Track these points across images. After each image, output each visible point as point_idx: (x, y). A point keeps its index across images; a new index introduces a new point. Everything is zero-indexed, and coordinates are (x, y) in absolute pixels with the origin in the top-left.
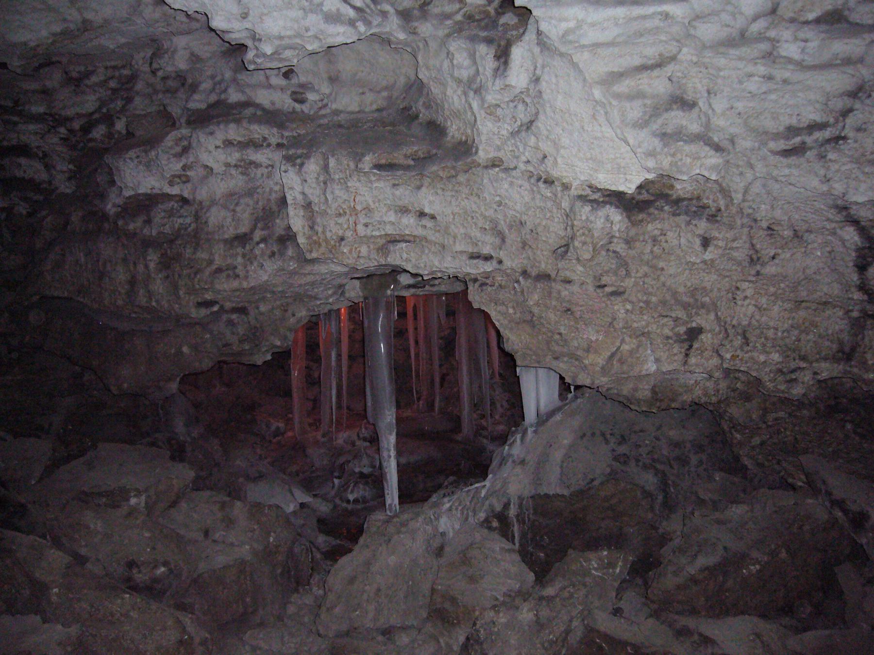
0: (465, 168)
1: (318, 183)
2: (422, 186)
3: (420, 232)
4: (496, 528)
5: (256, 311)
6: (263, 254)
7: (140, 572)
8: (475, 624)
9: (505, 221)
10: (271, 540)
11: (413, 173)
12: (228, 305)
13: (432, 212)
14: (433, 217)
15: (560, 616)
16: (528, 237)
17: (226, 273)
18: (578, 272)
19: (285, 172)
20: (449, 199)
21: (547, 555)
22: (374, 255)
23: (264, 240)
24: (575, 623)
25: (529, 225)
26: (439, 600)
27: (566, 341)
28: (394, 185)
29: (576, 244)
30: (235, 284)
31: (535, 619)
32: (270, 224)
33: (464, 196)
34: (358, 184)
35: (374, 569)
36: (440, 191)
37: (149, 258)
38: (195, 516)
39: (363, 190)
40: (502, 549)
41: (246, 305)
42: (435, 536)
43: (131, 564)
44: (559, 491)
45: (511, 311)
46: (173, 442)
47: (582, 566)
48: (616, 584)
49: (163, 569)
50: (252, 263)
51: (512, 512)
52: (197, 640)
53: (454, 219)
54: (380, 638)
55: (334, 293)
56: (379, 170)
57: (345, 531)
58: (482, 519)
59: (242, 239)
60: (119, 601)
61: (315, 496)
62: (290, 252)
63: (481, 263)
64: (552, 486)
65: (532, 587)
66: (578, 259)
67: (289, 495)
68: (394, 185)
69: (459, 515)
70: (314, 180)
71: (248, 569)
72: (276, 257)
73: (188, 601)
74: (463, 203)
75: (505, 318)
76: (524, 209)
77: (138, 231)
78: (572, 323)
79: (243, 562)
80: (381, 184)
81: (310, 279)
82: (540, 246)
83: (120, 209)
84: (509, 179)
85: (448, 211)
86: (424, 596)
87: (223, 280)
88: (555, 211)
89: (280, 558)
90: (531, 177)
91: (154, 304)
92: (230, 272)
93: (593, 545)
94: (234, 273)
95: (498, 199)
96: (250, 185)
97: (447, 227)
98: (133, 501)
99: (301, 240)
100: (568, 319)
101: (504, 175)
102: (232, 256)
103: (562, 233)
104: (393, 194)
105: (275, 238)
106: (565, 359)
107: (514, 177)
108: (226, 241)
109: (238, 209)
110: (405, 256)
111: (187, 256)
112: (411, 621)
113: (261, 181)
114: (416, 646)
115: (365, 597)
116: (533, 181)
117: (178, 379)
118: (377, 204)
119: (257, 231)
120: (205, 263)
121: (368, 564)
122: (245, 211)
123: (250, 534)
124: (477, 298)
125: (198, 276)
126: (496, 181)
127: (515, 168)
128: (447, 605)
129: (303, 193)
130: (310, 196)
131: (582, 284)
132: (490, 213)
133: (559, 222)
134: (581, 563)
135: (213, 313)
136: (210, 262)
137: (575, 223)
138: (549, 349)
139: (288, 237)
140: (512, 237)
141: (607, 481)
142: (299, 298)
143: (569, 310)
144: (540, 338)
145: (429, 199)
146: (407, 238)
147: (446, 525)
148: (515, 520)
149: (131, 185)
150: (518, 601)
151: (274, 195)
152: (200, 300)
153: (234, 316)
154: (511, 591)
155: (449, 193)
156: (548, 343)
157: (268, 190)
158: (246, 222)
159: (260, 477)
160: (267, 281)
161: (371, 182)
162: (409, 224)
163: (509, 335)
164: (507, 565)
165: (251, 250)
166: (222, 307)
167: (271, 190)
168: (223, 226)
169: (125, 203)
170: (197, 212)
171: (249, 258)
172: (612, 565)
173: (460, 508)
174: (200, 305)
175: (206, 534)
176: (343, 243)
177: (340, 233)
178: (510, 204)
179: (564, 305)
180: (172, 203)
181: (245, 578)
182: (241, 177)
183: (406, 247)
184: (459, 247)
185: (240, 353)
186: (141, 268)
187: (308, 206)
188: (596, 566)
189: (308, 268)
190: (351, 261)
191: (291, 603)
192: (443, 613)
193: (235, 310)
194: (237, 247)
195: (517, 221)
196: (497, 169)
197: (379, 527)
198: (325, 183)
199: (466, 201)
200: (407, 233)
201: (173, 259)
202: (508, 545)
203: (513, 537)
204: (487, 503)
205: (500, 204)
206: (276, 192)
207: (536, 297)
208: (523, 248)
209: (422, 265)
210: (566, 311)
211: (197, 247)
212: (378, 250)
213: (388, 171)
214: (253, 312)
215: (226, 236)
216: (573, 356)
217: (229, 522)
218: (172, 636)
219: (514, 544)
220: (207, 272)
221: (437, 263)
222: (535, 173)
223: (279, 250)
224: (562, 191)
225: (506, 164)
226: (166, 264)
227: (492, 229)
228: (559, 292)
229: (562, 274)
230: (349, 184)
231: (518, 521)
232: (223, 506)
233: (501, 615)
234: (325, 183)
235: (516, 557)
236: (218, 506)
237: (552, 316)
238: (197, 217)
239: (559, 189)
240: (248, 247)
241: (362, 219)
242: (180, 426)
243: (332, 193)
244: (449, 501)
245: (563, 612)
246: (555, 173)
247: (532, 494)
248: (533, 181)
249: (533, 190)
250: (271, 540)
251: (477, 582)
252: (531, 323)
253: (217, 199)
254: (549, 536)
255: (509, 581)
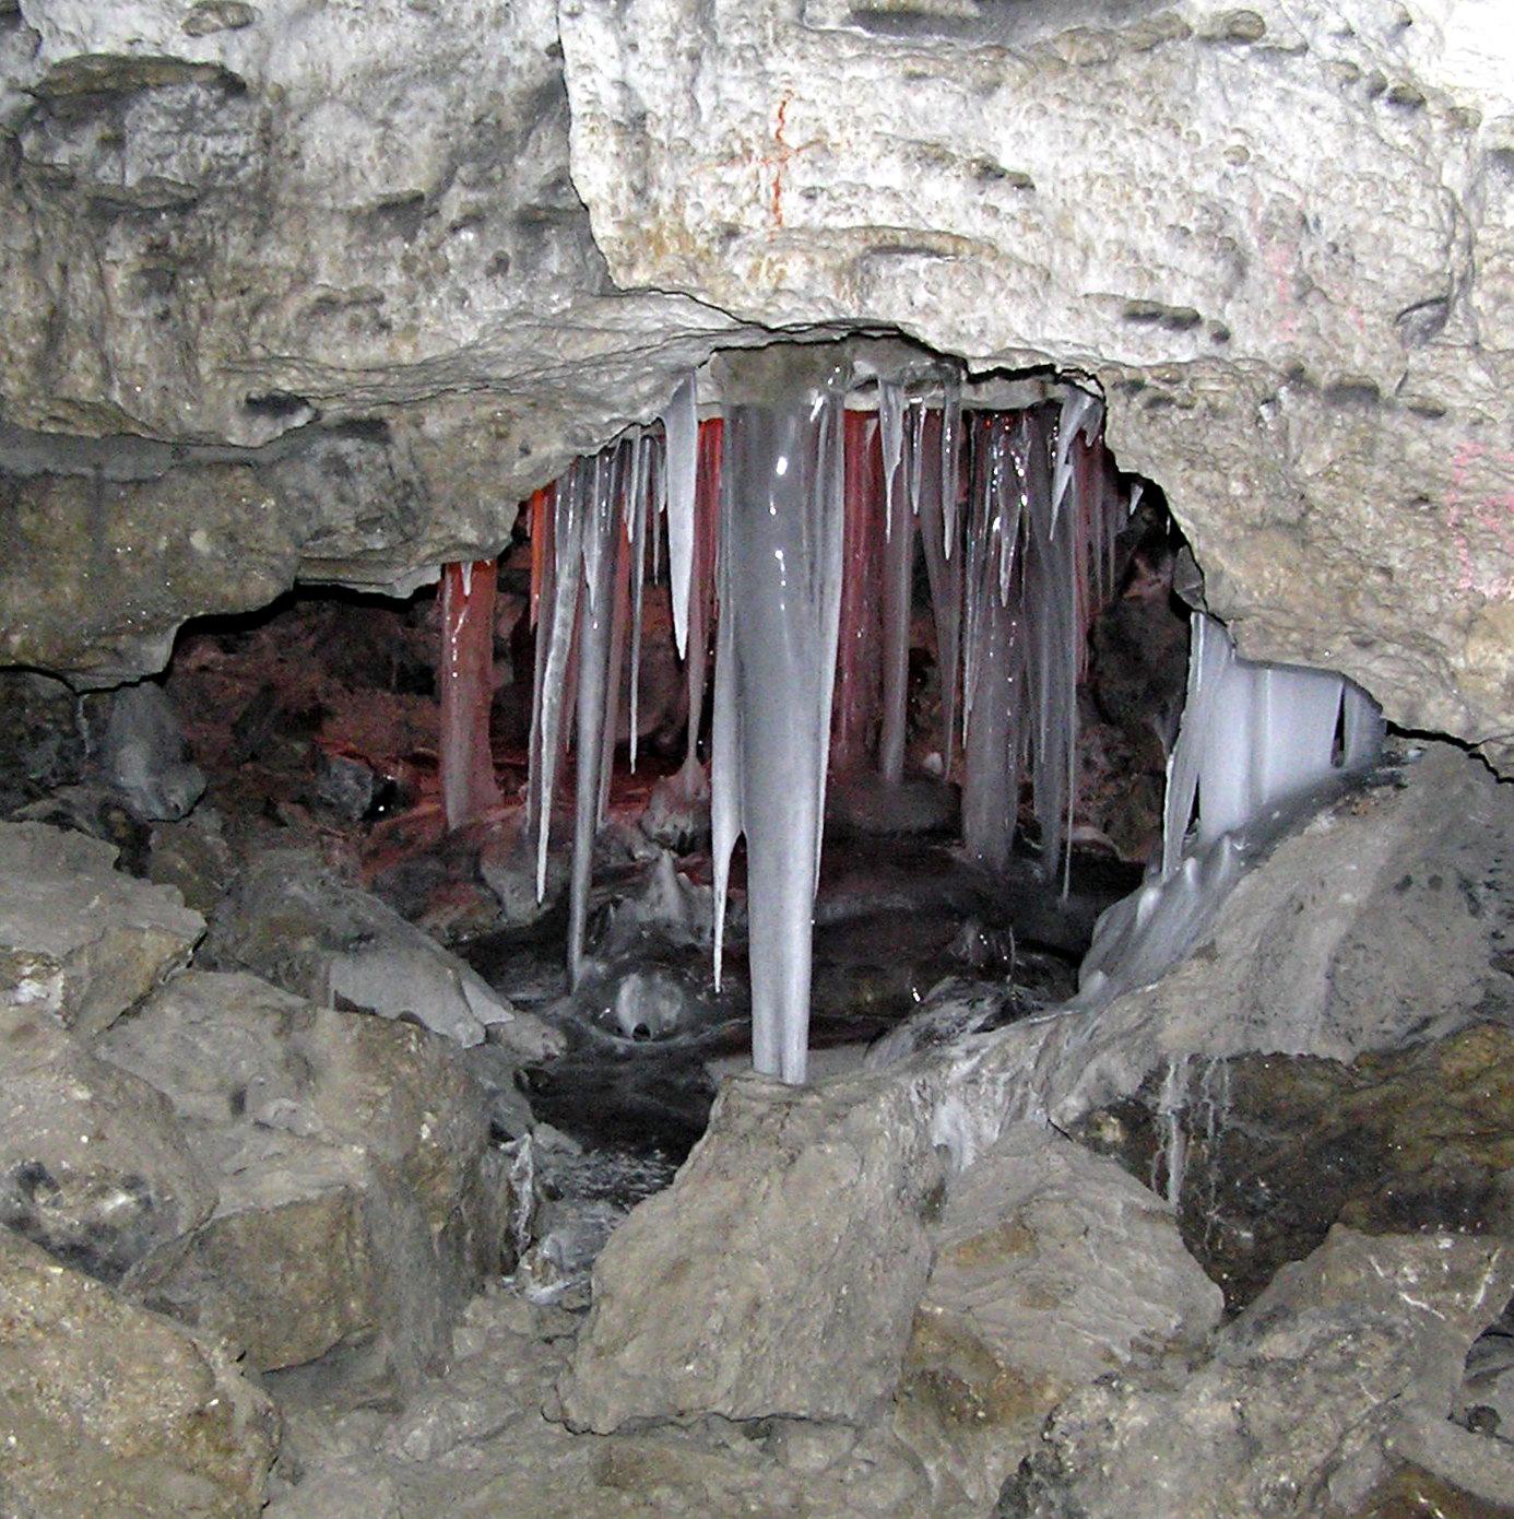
0: (1141, 38)
1: (673, 57)
2: (998, 85)
3: (976, 226)
4: (1113, 1147)
5: (413, 433)
6: (469, 262)
7: (55, 1204)
8: (1050, 1424)
9: (1251, 211)
10: (425, 1133)
11: (976, 45)
12: (334, 411)
13: (1021, 167)
14: (1023, 184)
15: (1315, 1418)
16: (1320, 265)
17: (350, 312)
18: (1470, 387)
19: (573, 15)
20: (1079, 130)
21: (1260, 1238)
22: (824, 287)
23: (474, 219)
24: (1352, 1445)
25: (1330, 231)
26: (934, 1345)
27: (1402, 593)
28: (912, 76)
29: (1477, 299)
30: (375, 350)
31: (1233, 1423)
32: (496, 172)
33: (1129, 125)
34: (796, 68)
35: (745, 1239)
36: (1053, 106)
37: (110, 255)
38: (204, 1046)
39: (810, 86)
40: (1130, 1209)
41: (385, 411)
42: (923, 1154)
43: (33, 1178)
44: (1323, 1050)
45: (1237, 488)
46: (115, 816)
47: (1372, 1277)
48: (1468, 1338)
49: (122, 1199)
50: (431, 288)
51: (1170, 1099)
52: (243, 1414)
53: (1089, 193)
54: (741, 1446)
55: (659, 391)
56: (869, 29)
57: (639, 1116)
58: (1071, 1117)
59: (406, 211)
60: (34, 1284)
61: (522, 1006)
62: (554, 262)
63: (1159, 333)
64: (1299, 1031)
65: (1216, 1329)
66: (1475, 346)
67: (456, 1000)
68: (912, 76)
69: (999, 1099)
70: (660, 47)
71: (358, 1218)
72: (511, 271)
73: (180, 1296)
74: (1122, 147)
75: (1215, 510)
76: (1315, 180)
77: (82, 170)
78: (1429, 541)
79: (348, 1195)
80: (871, 71)
81: (599, 346)
82: (1355, 295)
83: (29, 100)
84: (1280, 83)
85: (1074, 167)
86: (878, 1333)
87: (340, 336)
88: (1416, 191)
89: (443, 1190)
90: (1351, 81)
91: (117, 396)
92: (363, 313)
93: (1404, 1214)
94: (376, 316)
95: (1236, 140)
96: (441, 44)
97: (1065, 218)
98: (28, 990)
99: (604, 228)
100: (1418, 526)
101: (1262, 70)
102: (372, 262)
103: (1431, 262)
104: (904, 103)
105: (508, 214)
106: (1391, 649)
107: (1295, 78)
108: (354, 217)
109: (399, 118)
110: (921, 296)
111: (231, 254)
112: (840, 1404)
113: (474, 35)
114: (849, 1477)
115: (715, 1322)
116: (1356, 93)
117: (173, 631)
118: (850, 132)
119: (454, 190)
120: (285, 282)
121: (725, 1225)
122: (420, 126)
123: (365, 1114)
124: (1133, 439)
125: (263, 319)
126: (1238, 86)
127: (1304, 49)
128: (960, 1366)
129: (623, 85)
130: (643, 93)
131: (1477, 423)
132: (1207, 183)
133: (1425, 229)
134: (1370, 1268)
135: (289, 433)
136: (303, 278)
137: (1481, 235)
138: (1345, 613)
139: (555, 215)
140: (1268, 263)
141: (1473, 1026)
142: (545, 397)
143: (1423, 499)
144: (1322, 577)
145: (1019, 130)
146: (934, 242)
147: (955, 1125)
148: (1174, 1126)
149: (71, 28)
150: (1173, 1369)
151: (512, 83)
152: (257, 392)
153: (347, 446)
154: (1151, 1335)
155: (1083, 114)
156: (1345, 596)
157: (493, 64)
158: (423, 160)
159: (361, 940)
160: (475, 345)
161: (839, 62)
162: (945, 201)
163: (1225, 563)
164: (1143, 1259)
165: (433, 249)
166: (318, 415)
167: (505, 62)
168: (348, 168)
169: (47, 83)
170: (267, 121)
171: (425, 274)
172: (1463, 1280)
173: (1004, 1077)
174: (255, 406)
175: (238, 1102)
176: (734, 246)
177: (729, 214)
178: (1275, 159)
179: (1412, 483)
180: (193, 90)
181: (350, 1239)
182: (411, 19)
183: (929, 270)
184: (1095, 282)
185: (358, 560)
186: (83, 281)
187: (634, 125)
188: (1413, 1280)
189: (606, 313)
190: (748, 305)
191: (464, 1324)
192: (943, 1387)
193: (351, 427)
194: (390, 236)
195: (1292, 213)
196: (1243, 50)
197: (761, 1119)
198: (694, 57)
199: (1134, 140)
200: (936, 224)
201: (189, 260)
202: (1146, 1199)
203: (1163, 1176)
204: (1091, 1071)
205: (1240, 156)
206: (519, 71)
207: (1326, 453)
208: (1301, 299)
209: (974, 330)
210: (1414, 503)
211: (263, 226)
212: (838, 272)
213: (898, 33)
214: (402, 436)
215: (357, 202)
216: (1416, 640)
217: (304, 1071)
218: (180, 1397)
219: (1166, 1197)
220: (294, 305)
221: (1020, 327)
222: (1367, 70)
223: (521, 254)
224: (1449, 132)
225: (1271, 35)
226: (162, 274)
227: (1207, 233)
228: (1401, 442)
229: (1416, 387)
230: (771, 65)
231: (1183, 1127)
232: (287, 1022)
233: (1132, 1404)
234: (694, 57)
235: (1171, 1236)
236: (274, 1020)
237: (1368, 514)
238: (268, 138)
239: (1438, 125)
240: (422, 238)
241: (800, 175)
242: (134, 769)
243: (716, 89)
244: (970, 1053)
245: (1322, 1407)
246: (1430, 74)
247: (1234, 1052)
248: (1356, 93)
249: (1352, 124)
250: (425, 1133)
251: (1056, 1303)
252: (1297, 530)
253: (335, 84)
254: (1272, 1184)
255: (1148, 1306)
